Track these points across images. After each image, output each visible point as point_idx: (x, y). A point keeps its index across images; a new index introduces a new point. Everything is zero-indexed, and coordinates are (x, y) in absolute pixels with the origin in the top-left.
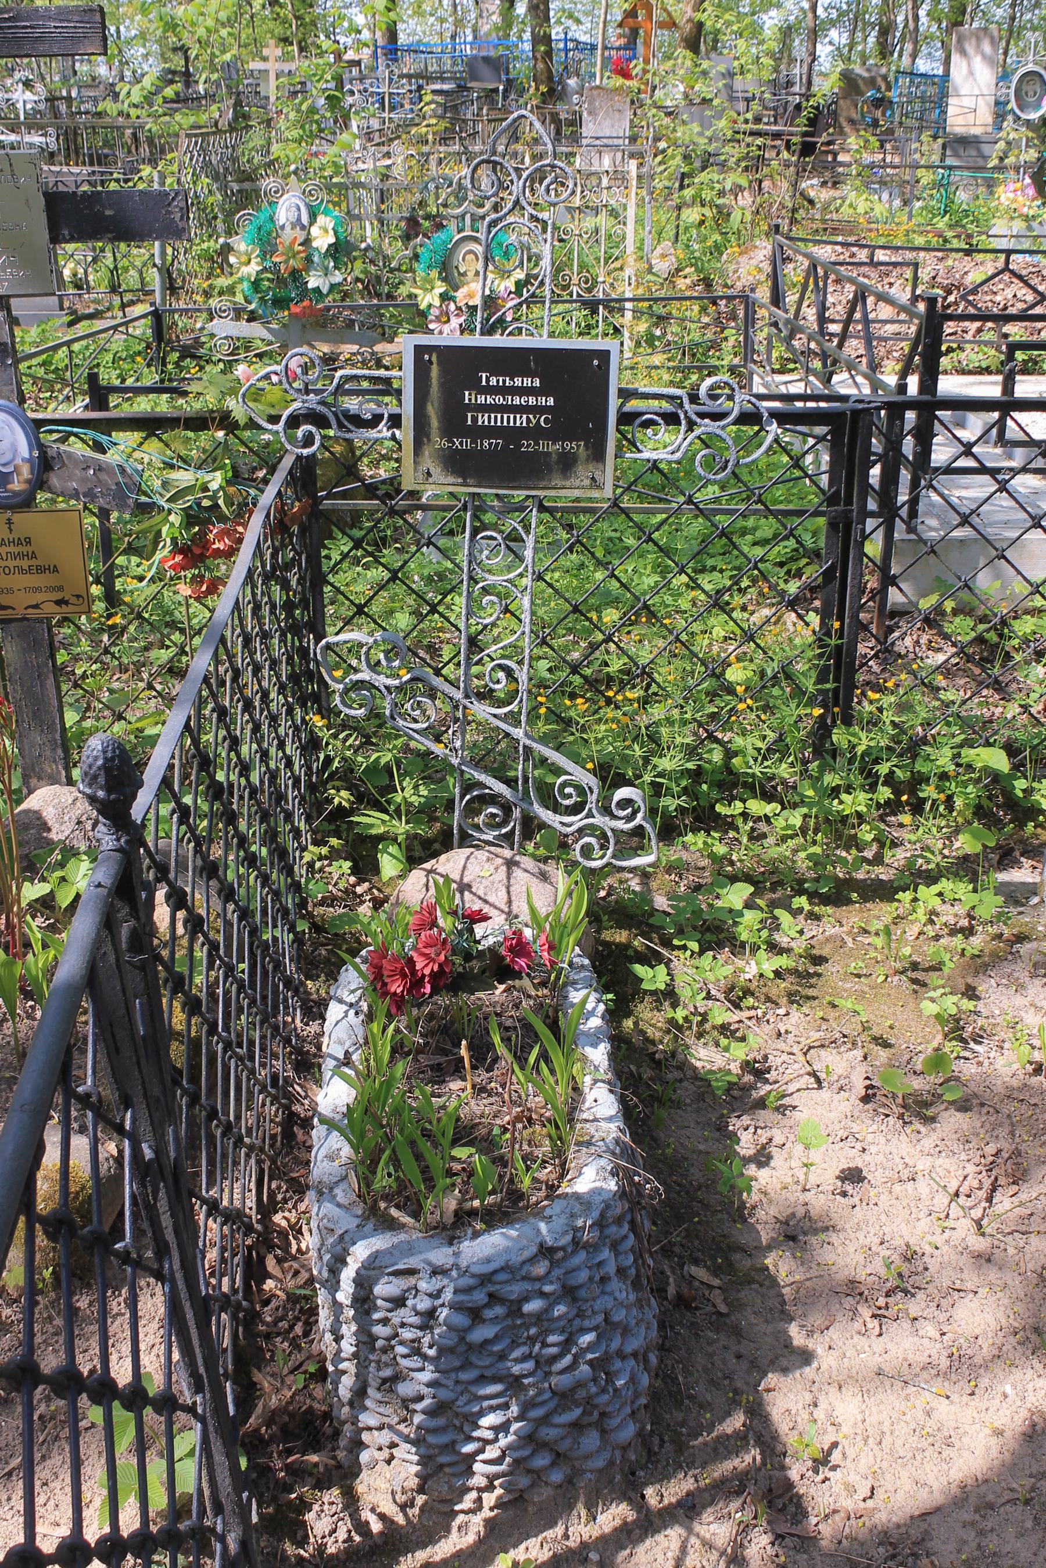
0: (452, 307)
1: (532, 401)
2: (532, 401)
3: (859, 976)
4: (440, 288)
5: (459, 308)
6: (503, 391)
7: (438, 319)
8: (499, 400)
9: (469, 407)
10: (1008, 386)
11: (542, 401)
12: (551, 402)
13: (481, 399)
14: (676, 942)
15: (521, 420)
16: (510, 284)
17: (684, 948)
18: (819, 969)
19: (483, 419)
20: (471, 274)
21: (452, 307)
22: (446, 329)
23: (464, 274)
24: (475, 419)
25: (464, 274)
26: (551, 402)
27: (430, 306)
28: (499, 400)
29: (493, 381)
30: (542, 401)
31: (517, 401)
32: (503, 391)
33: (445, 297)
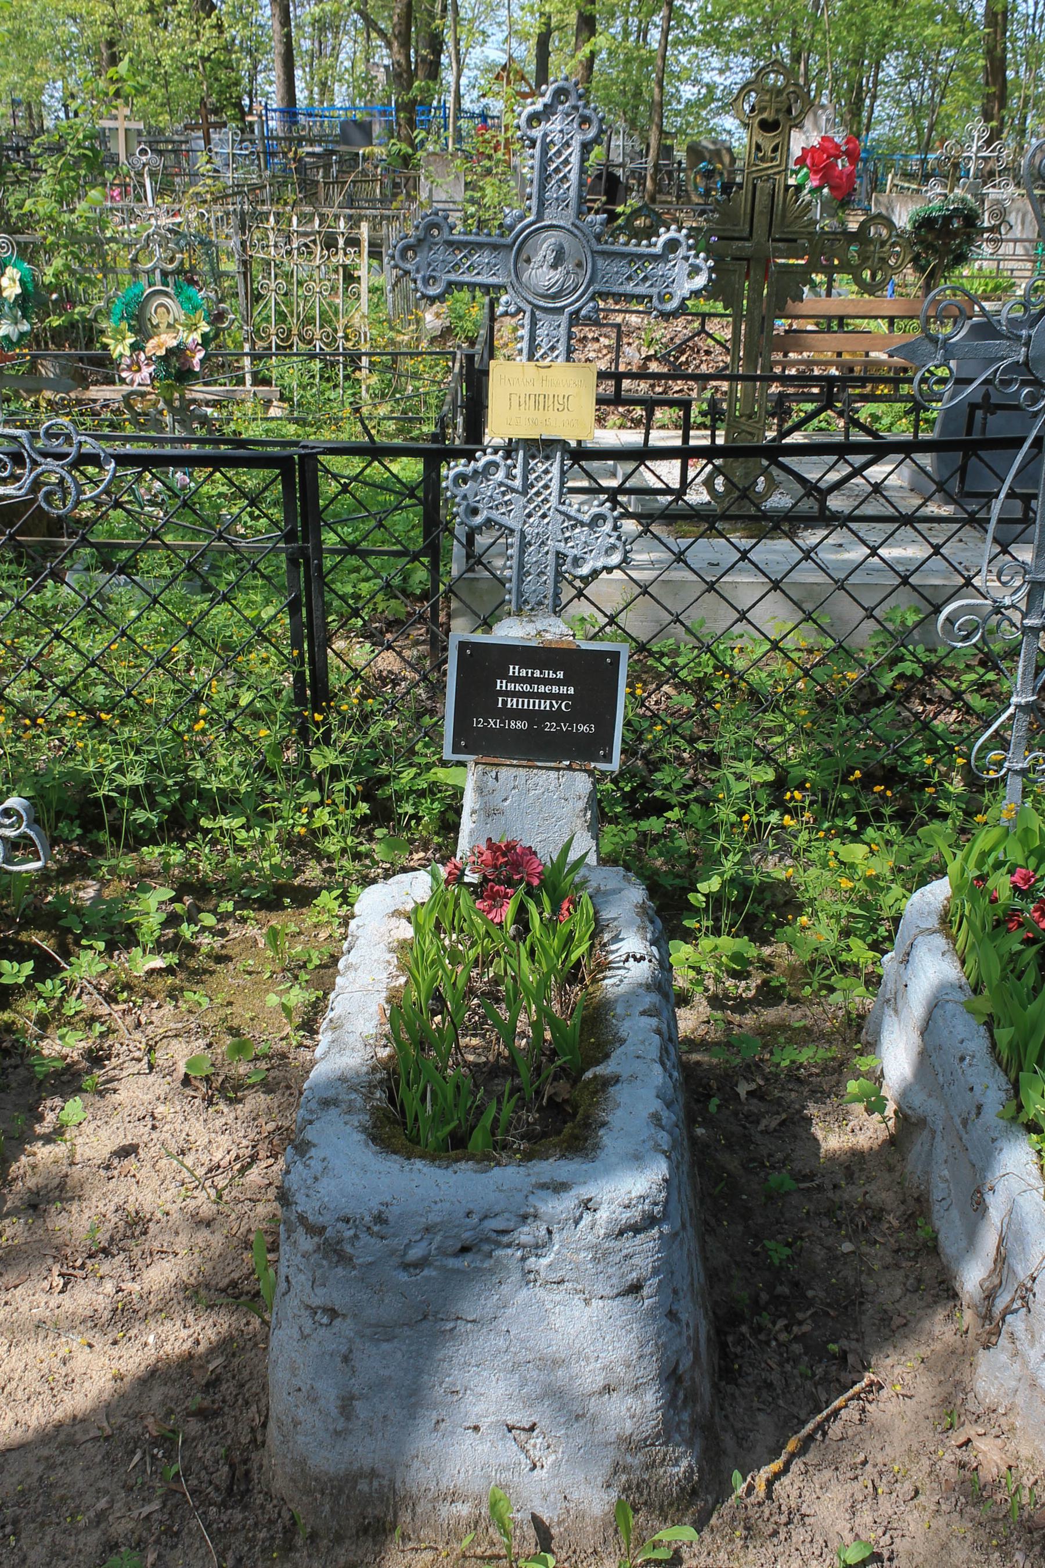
0: (142, 357)
1: (555, 689)
2: (555, 689)
3: (250, 973)
4: (131, 339)
5: (149, 358)
6: (531, 680)
7: (129, 368)
8: (527, 688)
9: (501, 693)
10: (686, 438)
11: (563, 690)
12: (571, 691)
13: (511, 687)
14: (84, 942)
15: (545, 705)
16: (197, 336)
17: (91, 947)
18: (219, 967)
19: (512, 703)
20: (163, 326)
21: (142, 357)
22: (138, 378)
23: (157, 326)
24: (505, 703)
25: (157, 326)
26: (571, 691)
27: (121, 355)
28: (527, 688)
29: (523, 673)
30: (563, 690)
31: (542, 689)
32: (531, 680)
33: (135, 347)
